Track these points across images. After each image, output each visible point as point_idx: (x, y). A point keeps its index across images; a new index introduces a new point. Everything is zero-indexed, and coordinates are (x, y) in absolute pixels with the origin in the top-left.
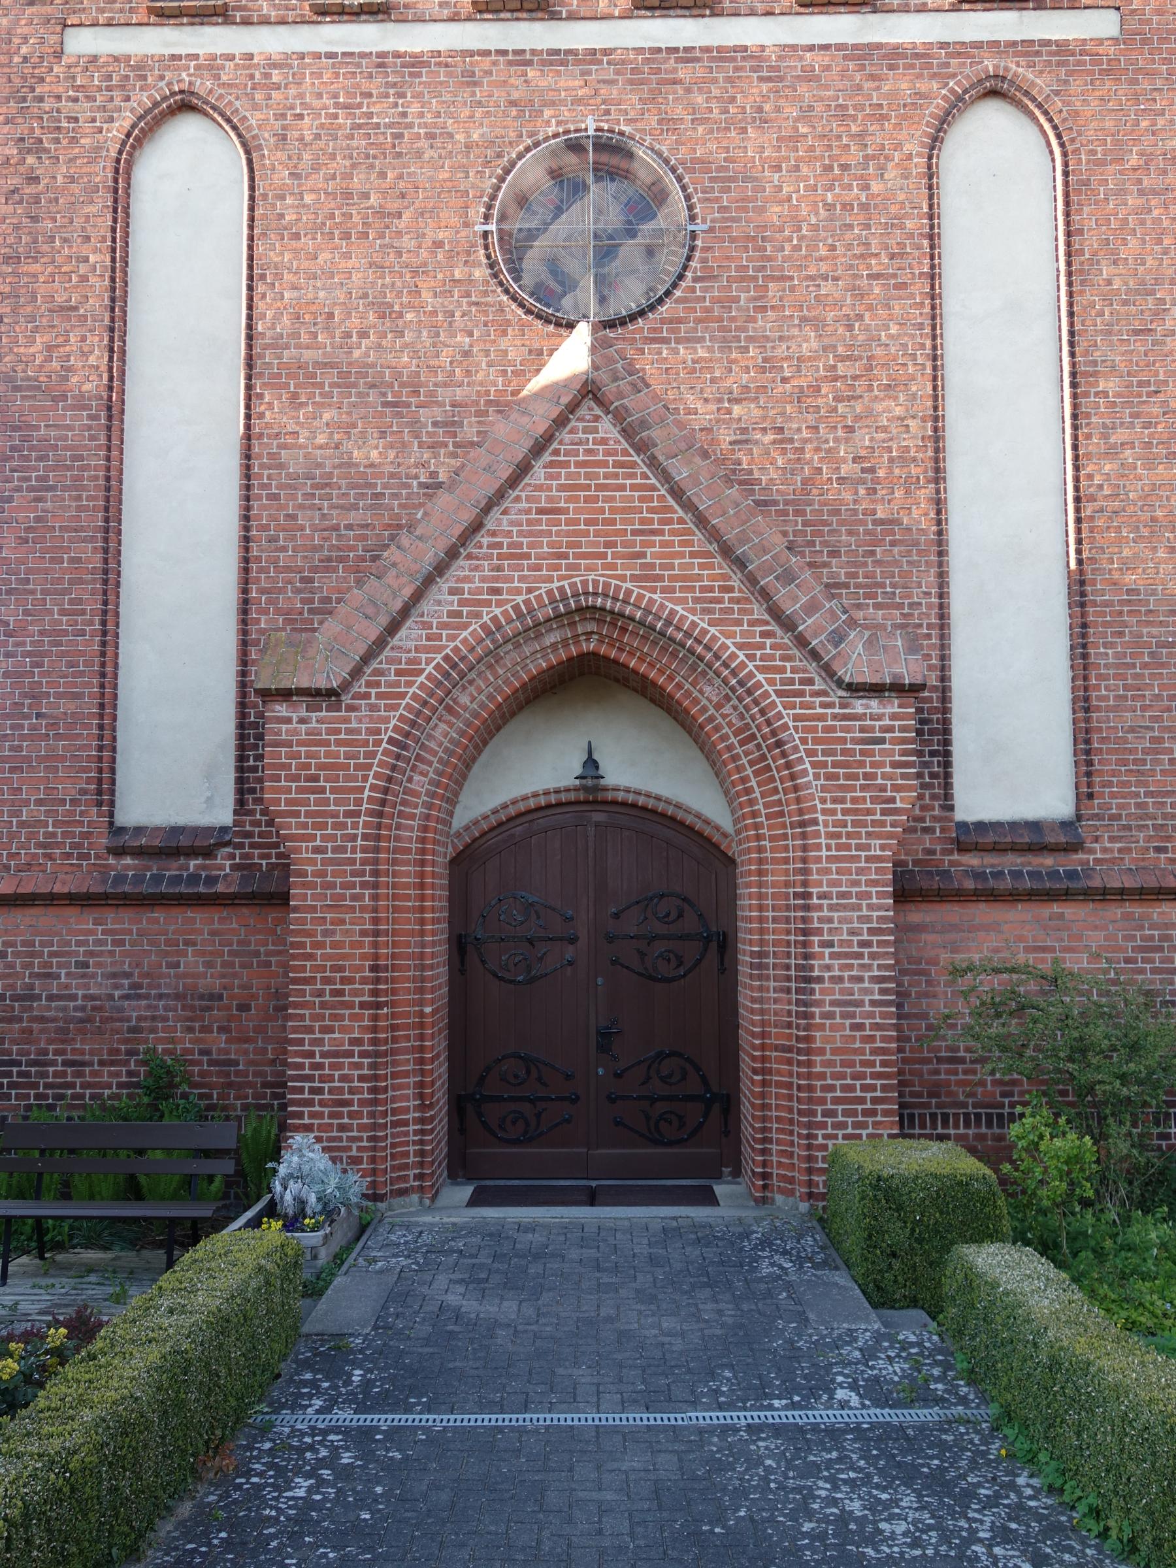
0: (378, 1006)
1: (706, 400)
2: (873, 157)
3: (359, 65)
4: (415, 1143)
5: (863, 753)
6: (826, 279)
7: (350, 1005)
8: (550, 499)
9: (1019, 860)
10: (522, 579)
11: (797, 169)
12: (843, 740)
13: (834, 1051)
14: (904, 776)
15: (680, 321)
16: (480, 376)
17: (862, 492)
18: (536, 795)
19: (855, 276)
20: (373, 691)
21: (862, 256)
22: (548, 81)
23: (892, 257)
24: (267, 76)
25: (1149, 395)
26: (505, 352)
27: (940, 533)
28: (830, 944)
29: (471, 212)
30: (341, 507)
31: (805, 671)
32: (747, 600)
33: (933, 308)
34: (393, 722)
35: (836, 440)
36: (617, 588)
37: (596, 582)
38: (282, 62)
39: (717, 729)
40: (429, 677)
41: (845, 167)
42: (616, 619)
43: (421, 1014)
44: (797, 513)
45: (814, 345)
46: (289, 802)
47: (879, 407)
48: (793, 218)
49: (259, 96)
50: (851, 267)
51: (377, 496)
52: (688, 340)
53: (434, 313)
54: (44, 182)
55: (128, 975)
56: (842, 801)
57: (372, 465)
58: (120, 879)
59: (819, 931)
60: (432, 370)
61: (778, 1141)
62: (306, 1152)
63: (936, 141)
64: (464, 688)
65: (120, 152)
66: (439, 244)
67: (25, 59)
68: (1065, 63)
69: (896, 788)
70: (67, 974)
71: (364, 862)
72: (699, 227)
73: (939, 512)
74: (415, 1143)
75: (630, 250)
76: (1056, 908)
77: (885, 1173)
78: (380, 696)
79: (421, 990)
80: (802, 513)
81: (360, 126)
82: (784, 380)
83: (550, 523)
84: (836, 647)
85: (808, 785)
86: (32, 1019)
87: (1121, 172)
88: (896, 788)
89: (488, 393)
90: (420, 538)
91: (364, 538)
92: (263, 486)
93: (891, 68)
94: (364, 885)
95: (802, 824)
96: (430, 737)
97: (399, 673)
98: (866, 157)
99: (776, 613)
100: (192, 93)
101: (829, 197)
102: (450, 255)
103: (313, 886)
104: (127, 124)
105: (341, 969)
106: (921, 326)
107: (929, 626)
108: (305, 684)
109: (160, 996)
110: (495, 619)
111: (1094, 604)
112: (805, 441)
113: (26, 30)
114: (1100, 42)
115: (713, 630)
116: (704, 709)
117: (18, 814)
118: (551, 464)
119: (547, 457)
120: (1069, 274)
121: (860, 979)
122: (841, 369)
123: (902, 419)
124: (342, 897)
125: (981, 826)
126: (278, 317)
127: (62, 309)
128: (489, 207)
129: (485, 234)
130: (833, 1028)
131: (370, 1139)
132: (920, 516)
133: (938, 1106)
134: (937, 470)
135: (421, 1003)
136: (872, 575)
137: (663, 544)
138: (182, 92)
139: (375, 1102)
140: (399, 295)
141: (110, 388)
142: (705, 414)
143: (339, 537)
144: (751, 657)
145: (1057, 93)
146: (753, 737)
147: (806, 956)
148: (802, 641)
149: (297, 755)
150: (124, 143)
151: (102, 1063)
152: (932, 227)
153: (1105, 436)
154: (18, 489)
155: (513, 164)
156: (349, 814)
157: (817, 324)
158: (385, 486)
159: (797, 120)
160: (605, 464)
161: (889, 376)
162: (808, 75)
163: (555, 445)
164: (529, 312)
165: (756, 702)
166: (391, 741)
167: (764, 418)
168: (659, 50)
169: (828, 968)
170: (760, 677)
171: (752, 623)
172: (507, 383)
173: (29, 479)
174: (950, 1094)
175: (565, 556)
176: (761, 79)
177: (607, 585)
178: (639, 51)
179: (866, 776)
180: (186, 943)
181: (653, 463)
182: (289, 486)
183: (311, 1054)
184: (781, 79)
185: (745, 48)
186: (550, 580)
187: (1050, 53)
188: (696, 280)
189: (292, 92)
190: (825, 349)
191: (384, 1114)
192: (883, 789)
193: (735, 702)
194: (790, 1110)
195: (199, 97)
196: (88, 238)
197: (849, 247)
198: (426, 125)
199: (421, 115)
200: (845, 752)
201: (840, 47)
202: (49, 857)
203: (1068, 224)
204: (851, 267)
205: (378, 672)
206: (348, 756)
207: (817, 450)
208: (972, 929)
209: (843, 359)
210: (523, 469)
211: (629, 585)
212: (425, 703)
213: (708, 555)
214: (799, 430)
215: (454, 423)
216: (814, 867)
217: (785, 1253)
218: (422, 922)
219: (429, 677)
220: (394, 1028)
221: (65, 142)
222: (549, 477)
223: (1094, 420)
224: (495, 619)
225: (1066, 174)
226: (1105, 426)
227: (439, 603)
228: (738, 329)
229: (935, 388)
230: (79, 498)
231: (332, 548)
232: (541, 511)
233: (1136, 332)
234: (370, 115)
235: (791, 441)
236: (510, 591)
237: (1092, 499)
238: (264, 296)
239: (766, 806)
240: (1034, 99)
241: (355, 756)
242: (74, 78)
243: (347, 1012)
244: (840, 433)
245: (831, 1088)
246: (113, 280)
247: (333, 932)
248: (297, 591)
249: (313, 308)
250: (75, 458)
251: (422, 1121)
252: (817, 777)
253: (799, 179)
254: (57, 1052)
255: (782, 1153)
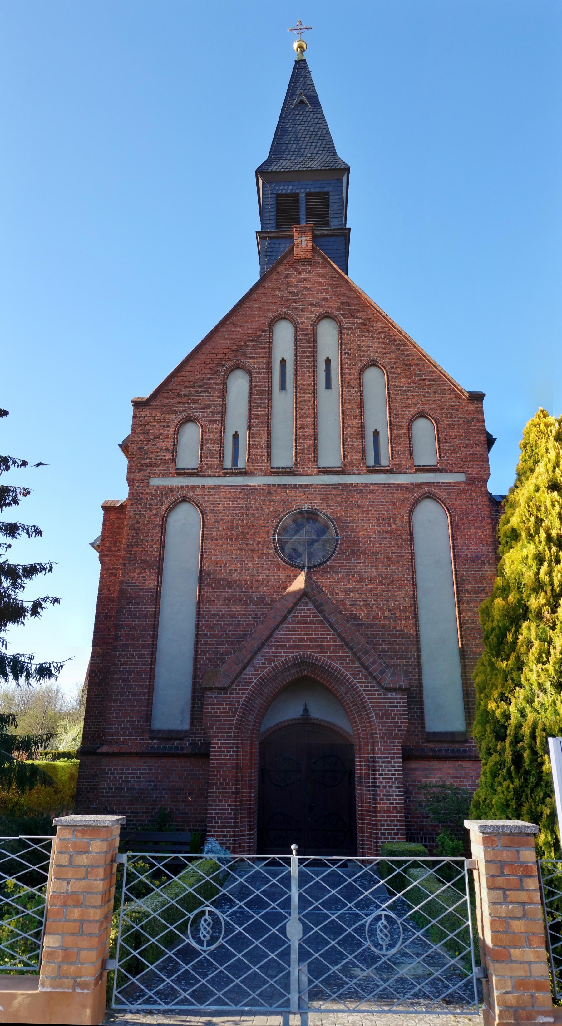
0: (237, 793)
1: (342, 591)
2: (392, 517)
3: (237, 489)
4: (247, 843)
5: (391, 710)
6: (378, 553)
7: (228, 793)
8: (293, 627)
9: (447, 746)
10: (284, 652)
11: (369, 520)
12: (385, 706)
13: (384, 812)
14: (404, 718)
15: (334, 566)
16: (271, 583)
17: (392, 621)
18: (288, 721)
19: (388, 553)
20: (238, 688)
21: (389, 547)
22: (294, 493)
23: (399, 547)
24: (209, 492)
25: (481, 591)
26: (279, 576)
27: (417, 634)
28: (382, 774)
29: (270, 533)
30: (227, 624)
31: (372, 683)
32: (354, 660)
33: (412, 563)
34: (244, 698)
35: (383, 604)
36: (314, 656)
37: (307, 654)
38: (214, 488)
39: (346, 701)
40: (255, 684)
41: (383, 520)
42: (313, 665)
43: (250, 797)
44: (371, 628)
45: (375, 574)
46: (211, 724)
47: (396, 594)
48: (368, 535)
49: (206, 498)
50: (386, 550)
51: (238, 621)
52: (336, 572)
53: (258, 563)
54: (141, 523)
55: (153, 781)
56: (385, 726)
57: (237, 611)
58: (153, 747)
59: (378, 770)
60: (257, 581)
61: (367, 845)
62: (213, 843)
63: (411, 512)
64: (266, 687)
65: (164, 514)
66: (259, 542)
67: (138, 487)
68: (450, 489)
69: (402, 722)
70: (134, 781)
71: (234, 744)
72: (339, 538)
73: (416, 628)
74: (247, 843)
75: (317, 546)
76: (460, 763)
77: (394, 850)
78: (239, 690)
79: (250, 788)
80: (373, 628)
81: (236, 507)
82: (366, 585)
83: (293, 635)
84: (381, 675)
85: (374, 721)
86: (121, 797)
87: (468, 522)
88: (402, 722)
89: (274, 588)
90: (253, 639)
91: (234, 634)
92: (203, 618)
93: (397, 490)
94: (233, 752)
95: (372, 734)
96: (255, 703)
97: (246, 682)
98: (390, 517)
99: (362, 664)
100: (187, 497)
101: (379, 529)
102: (263, 546)
103: (217, 751)
104: (167, 506)
105: (226, 780)
106: (408, 569)
107: (415, 665)
108: (217, 686)
109: (164, 789)
110: (275, 665)
111: (468, 658)
112: (373, 604)
113: (138, 479)
114: (460, 482)
115: (343, 670)
116: (341, 695)
117: (121, 725)
118: (293, 616)
119: (292, 614)
120: (454, 553)
121: (392, 787)
122: (384, 582)
123: (404, 598)
124: (227, 756)
125: (435, 734)
126: (210, 564)
127: (144, 561)
128: (275, 531)
129: (274, 539)
130: (384, 804)
131: (233, 840)
132: (410, 629)
133: (424, 834)
134: (415, 614)
135: (250, 792)
136: (396, 648)
137: (328, 642)
138: (183, 497)
139: (235, 827)
140: (247, 558)
141: (157, 586)
142: (342, 595)
143: (227, 634)
144: (355, 679)
145: (447, 498)
146: (357, 704)
147: (374, 779)
148: (370, 674)
149: (213, 709)
150: (166, 512)
151: (143, 813)
152: (411, 538)
153: (468, 604)
154: (127, 618)
155: (282, 518)
156: (229, 728)
157: (376, 567)
158: (241, 618)
159: (368, 505)
160: (309, 617)
161: (399, 584)
162: (372, 493)
163: (294, 611)
164: (287, 563)
165: (357, 693)
166: (243, 704)
167: (360, 597)
168: (326, 485)
169: (382, 783)
170: (358, 685)
171: (355, 667)
172: (280, 585)
173: (131, 615)
174: (427, 830)
175: (297, 645)
176: (357, 493)
177: (310, 655)
178: (320, 485)
179: (392, 718)
180: (173, 770)
181: (324, 616)
182: (212, 618)
183: (215, 810)
184: (363, 493)
185: (352, 484)
186: (293, 653)
187: (444, 486)
188: (338, 554)
189: (216, 497)
190: (379, 575)
191: (238, 832)
192: (398, 722)
193: (351, 692)
194: (370, 833)
195: (188, 498)
196: (153, 540)
197: (385, 544)
198: (256, 507)
199: (255, 504)
200: (385, 710)
201: (381, 484)
202: (130, 739)
203: (453, 537)
204: (386, 550)
205: (240, 682)
206: (229, 709)
207: (377, 607)
208: (433, 770)
209: (384, 579)
210: (285, 618)
211: (317, 655)
212: (254, 692)
213: (341, 645)
214: (371, 601)
215: (263, 598)
216: (376, 748)
217: (366, 880)
218: (251, 764)
219: (255, 684)
220: (242, 801)
221: (148, 511)
222: (293, 620)
223: (464, 598)
224: (275, 665)
225: (451, 522)
226: (468, 600)
227: (258, 660)
228: (351, 569)
229: (414, 588)
230: (146, 621)
231: (224, 638)
232: (290, 631)
233: (476, 571)
234: (239, 504)
235: (369, 604)
236: (281, 656)
237: (465, 624)
238: (206, 558)
239: (362, 727)
240: (440, 500)
241: (231, 709)
242: (152, 493)
243: (227, 795)
244: (384, 602)
245: (383, 825)
246: (160, 553)
247: (223, 768)
248: (213, 651)
249: (221, 562)
250: (145, 608)
251: (249, 835)
252: (376, 718)
253: (369, 523)
254: (128, 809)
255: (368, 849)
